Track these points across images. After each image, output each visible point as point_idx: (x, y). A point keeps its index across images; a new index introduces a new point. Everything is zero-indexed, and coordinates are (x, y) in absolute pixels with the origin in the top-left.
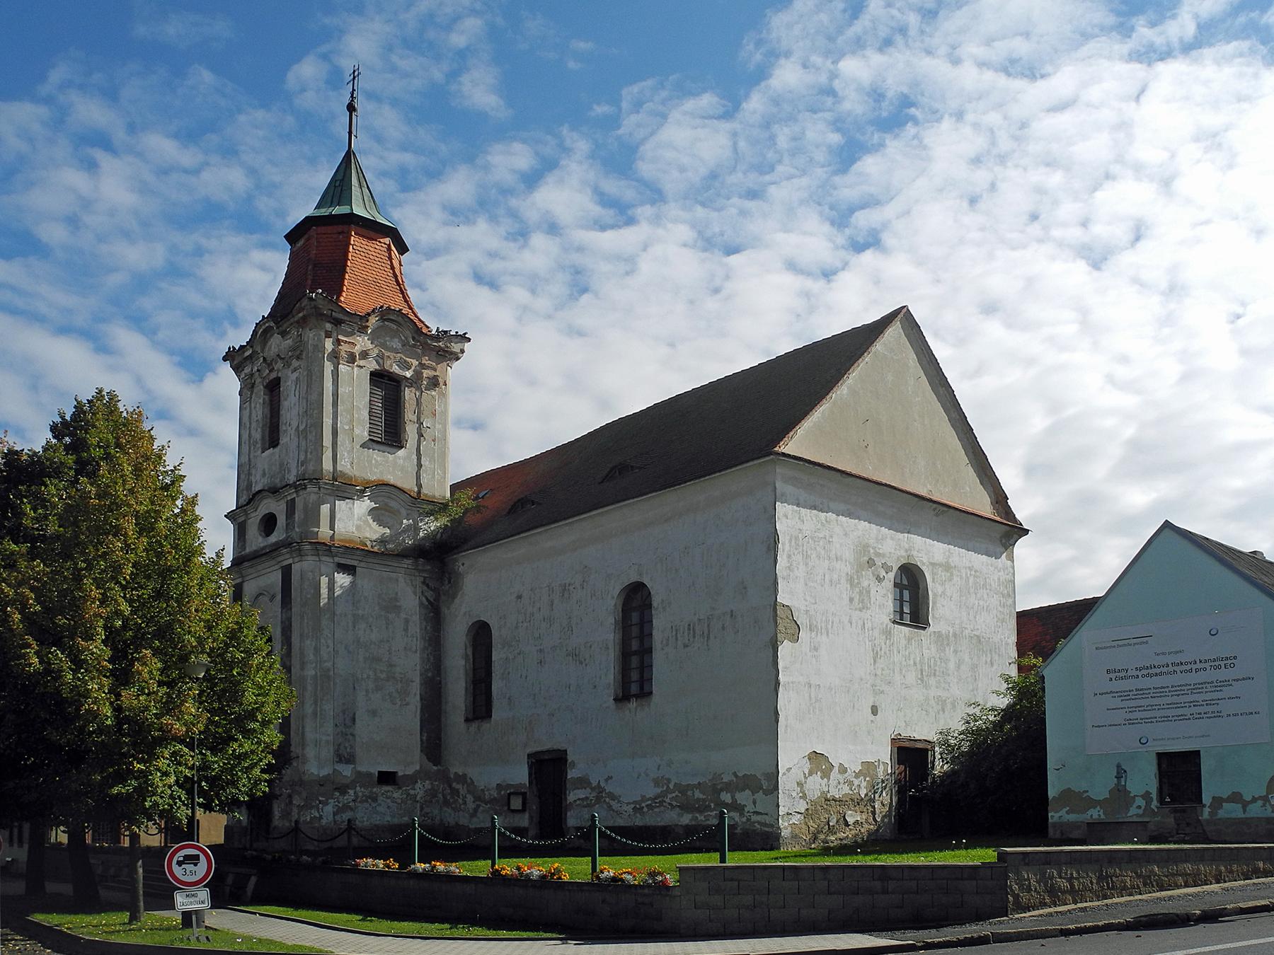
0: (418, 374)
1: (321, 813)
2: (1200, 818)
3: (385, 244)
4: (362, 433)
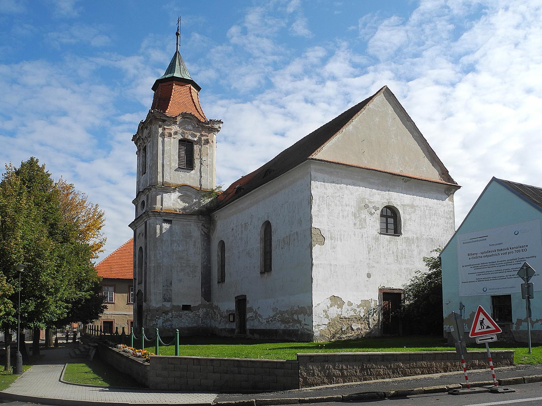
0: (200, 139)
1: (157, 323)
2: (511, 330)
3: (188, 87)
4: (175, 165)
